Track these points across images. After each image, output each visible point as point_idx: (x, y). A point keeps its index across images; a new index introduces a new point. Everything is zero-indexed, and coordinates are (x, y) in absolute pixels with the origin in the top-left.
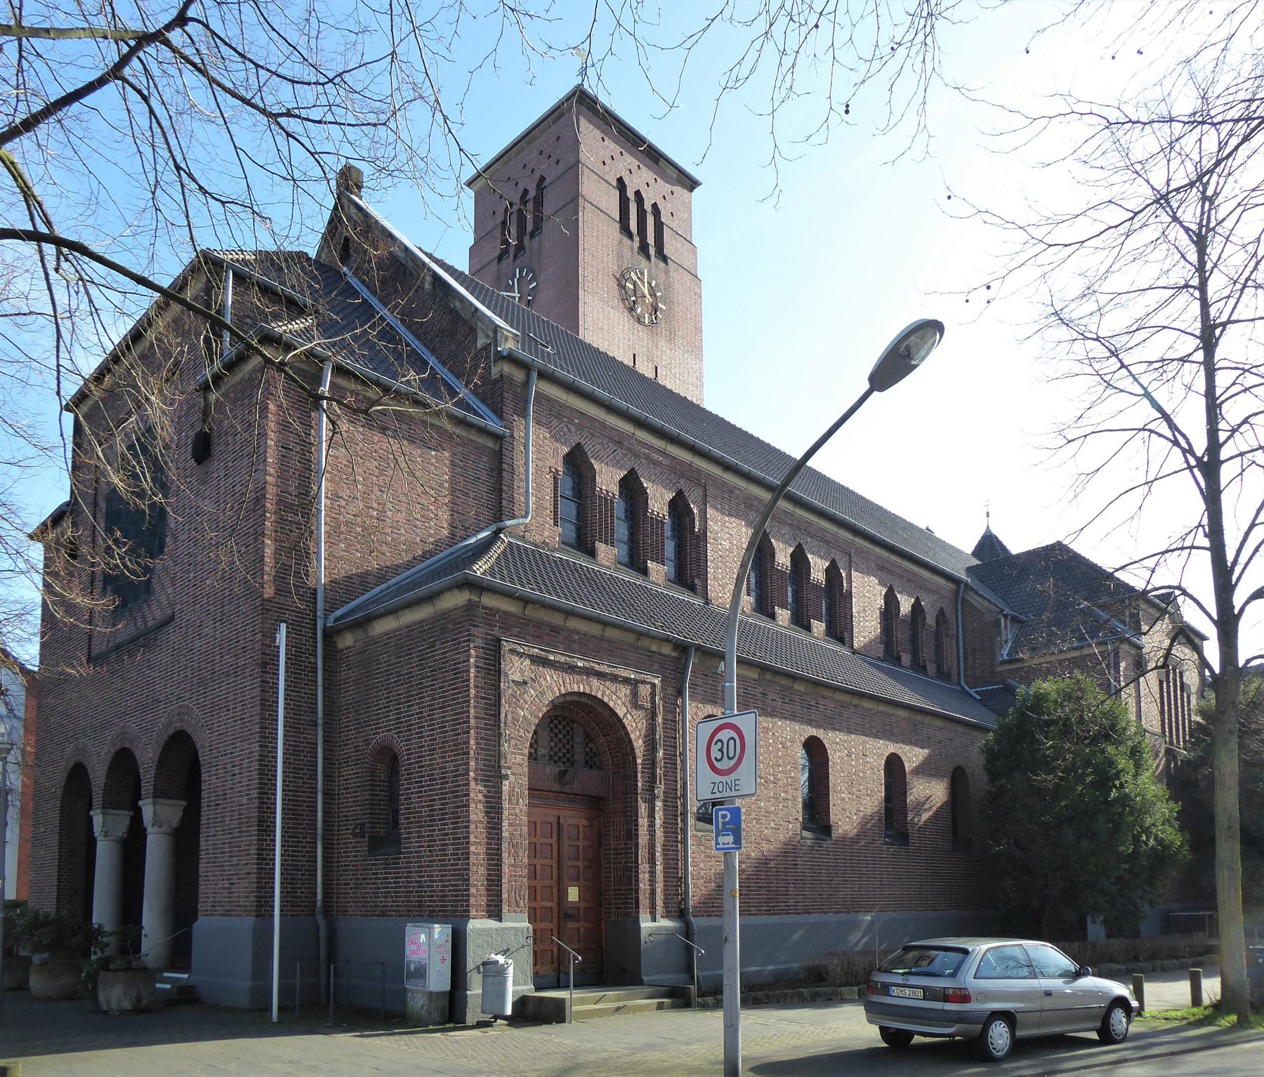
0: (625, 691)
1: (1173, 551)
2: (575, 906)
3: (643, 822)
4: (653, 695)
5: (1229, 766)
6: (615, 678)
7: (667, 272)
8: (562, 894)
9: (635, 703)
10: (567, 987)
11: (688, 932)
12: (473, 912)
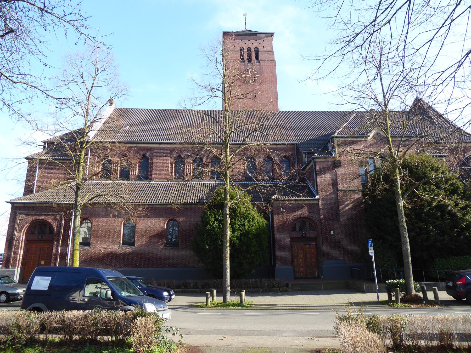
0: (52, 217)
4: (61, 217)
6: (49, 215)
9: (55, 219)
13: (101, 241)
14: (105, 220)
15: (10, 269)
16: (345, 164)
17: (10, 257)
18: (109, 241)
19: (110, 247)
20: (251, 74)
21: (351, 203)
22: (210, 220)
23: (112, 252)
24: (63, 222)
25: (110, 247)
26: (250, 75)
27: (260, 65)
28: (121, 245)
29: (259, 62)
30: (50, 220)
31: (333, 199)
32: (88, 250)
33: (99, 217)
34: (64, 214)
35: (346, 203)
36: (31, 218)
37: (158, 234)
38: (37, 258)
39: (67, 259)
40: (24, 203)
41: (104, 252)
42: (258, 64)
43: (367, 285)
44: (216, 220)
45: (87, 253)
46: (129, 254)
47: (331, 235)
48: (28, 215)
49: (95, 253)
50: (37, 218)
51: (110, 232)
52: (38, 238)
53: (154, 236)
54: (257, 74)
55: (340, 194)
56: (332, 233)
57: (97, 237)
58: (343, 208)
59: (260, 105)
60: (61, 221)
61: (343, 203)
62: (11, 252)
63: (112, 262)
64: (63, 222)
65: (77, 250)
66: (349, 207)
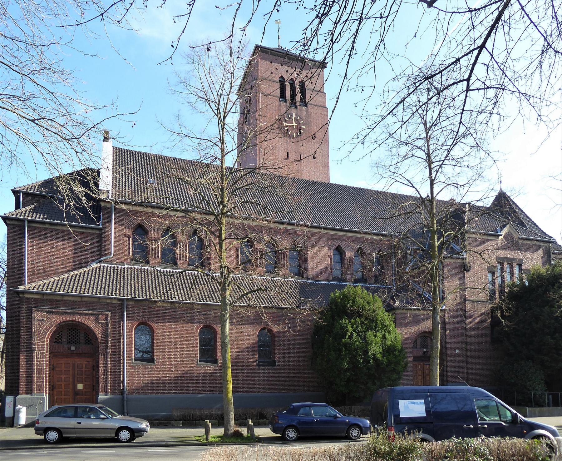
0: (92, 318)
1: (494, 88)
2: (80, 390)
3: (101, 363)
4: (106, 318)
5: (524, 276)
6: (86, 314)
7: (307, 111)
8: (75, 386)
9: (97, 321)
10: (27, 415)
11: (123, 400)
12: (21, 392)
13: (170, 356)
14: (173, 325)
15: (35, 396)
16: (475, 267)
17: (32, 377)
18: (181, 356)
19: (184, 365)
20: (296, 123)
21: (479, 317)
22: (347, 331)
23: (187, 372)
24: (110, 326)
25: (184, 365)
26: (294, 124)
27: (307, 111)
28: (133, 361)
29: (306, 106)
30: (89, 322)
31: (461, 312)
32: (152, 369)
33: (163, 321)
34: (109, 314)
35: (474, 317)
36: (57, 319)
37: (248, 348)
38: (71, 380)
39: (123, 382)
40: (43, 294)
41: (175, 372)
42: (304, 108)
43: (530, 409)
44: (354, 330)
45: (151, 372)
46: (210, 375)
47: (455, 354)
48: (53, 313)
49: (163, 372)
50: (68, 319)
51: (181, 344)
52: (70, 349)
53: (243, 350)
54: (303, 124)
55: (468, 305)
56: (457, 351)
57: (163, 350)
58: (471, 322)
59: (309, 172)
60: (107, 325)
61: (471, 316)
62: (32, 370)
63: (187, 386)
64: (110, 326)
65: (229, 367)
66: (476, 321)
